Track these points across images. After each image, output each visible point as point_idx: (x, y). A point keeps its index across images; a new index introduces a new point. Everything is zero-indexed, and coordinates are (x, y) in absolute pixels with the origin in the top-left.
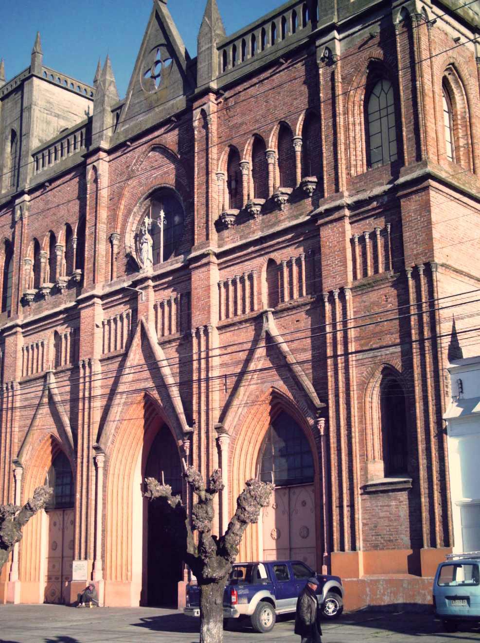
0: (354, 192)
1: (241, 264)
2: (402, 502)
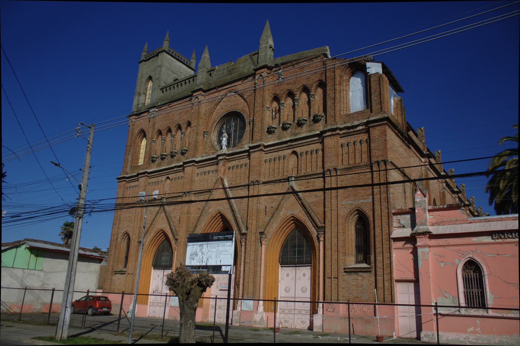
0: (343, 122)
1: (278, 152)
2: (365, 278)
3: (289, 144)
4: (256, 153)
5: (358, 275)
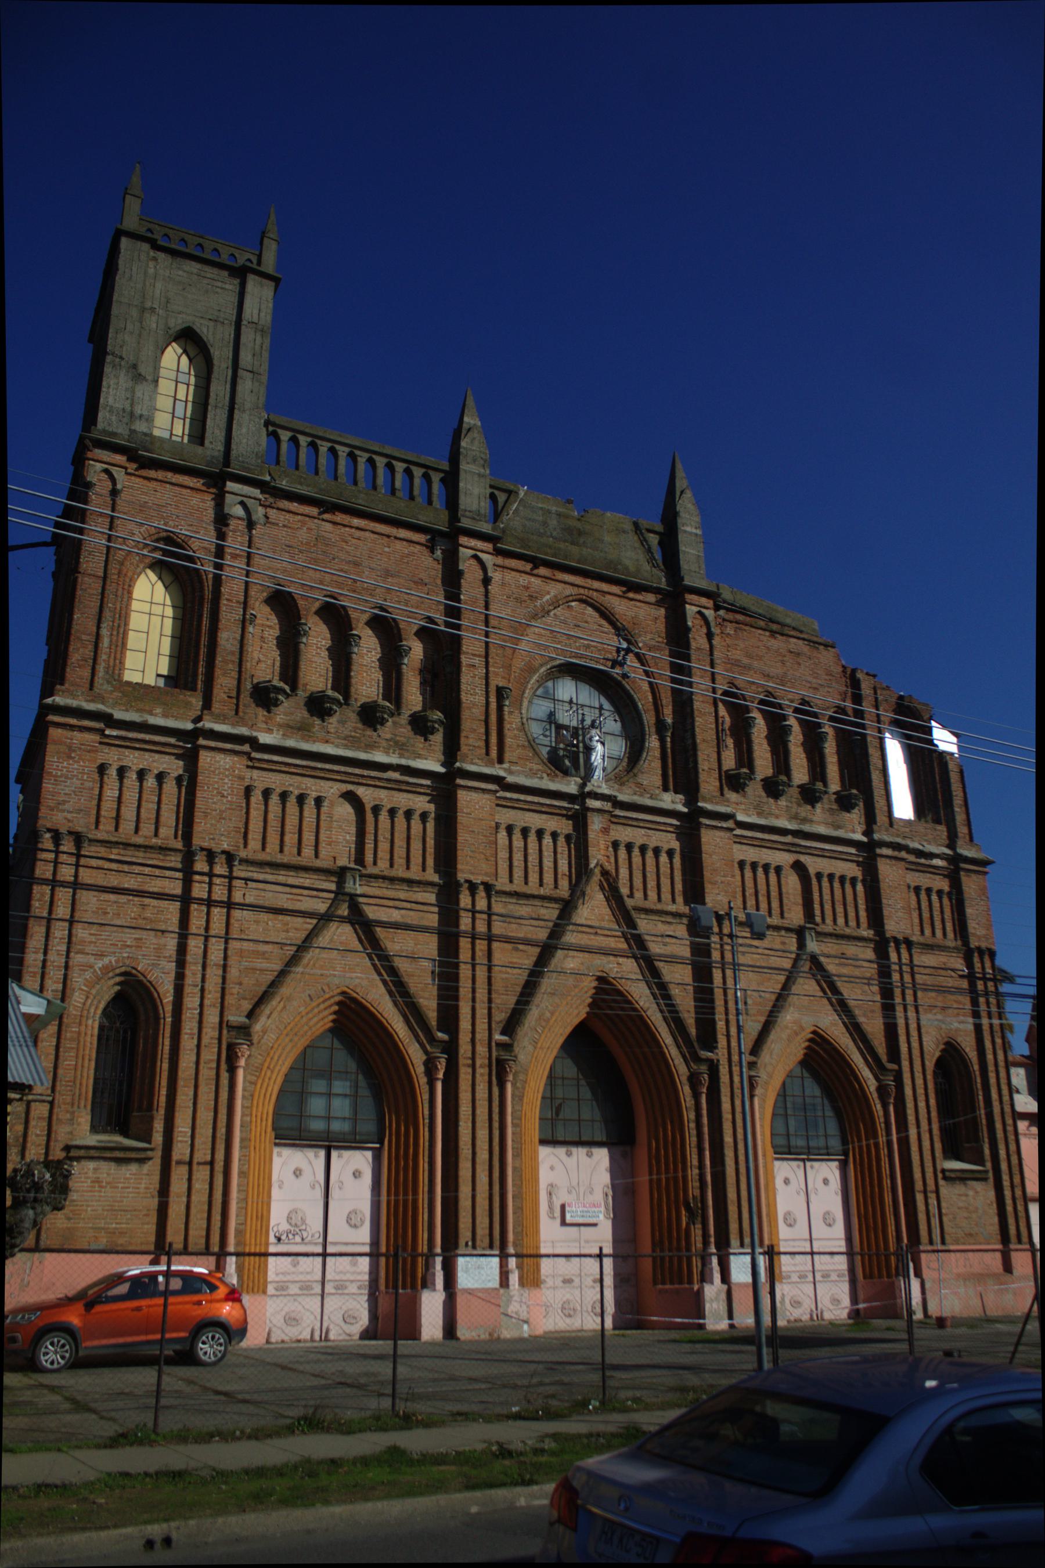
3: (789, 839)
4: (718, 833)
5: (965, 1184)
